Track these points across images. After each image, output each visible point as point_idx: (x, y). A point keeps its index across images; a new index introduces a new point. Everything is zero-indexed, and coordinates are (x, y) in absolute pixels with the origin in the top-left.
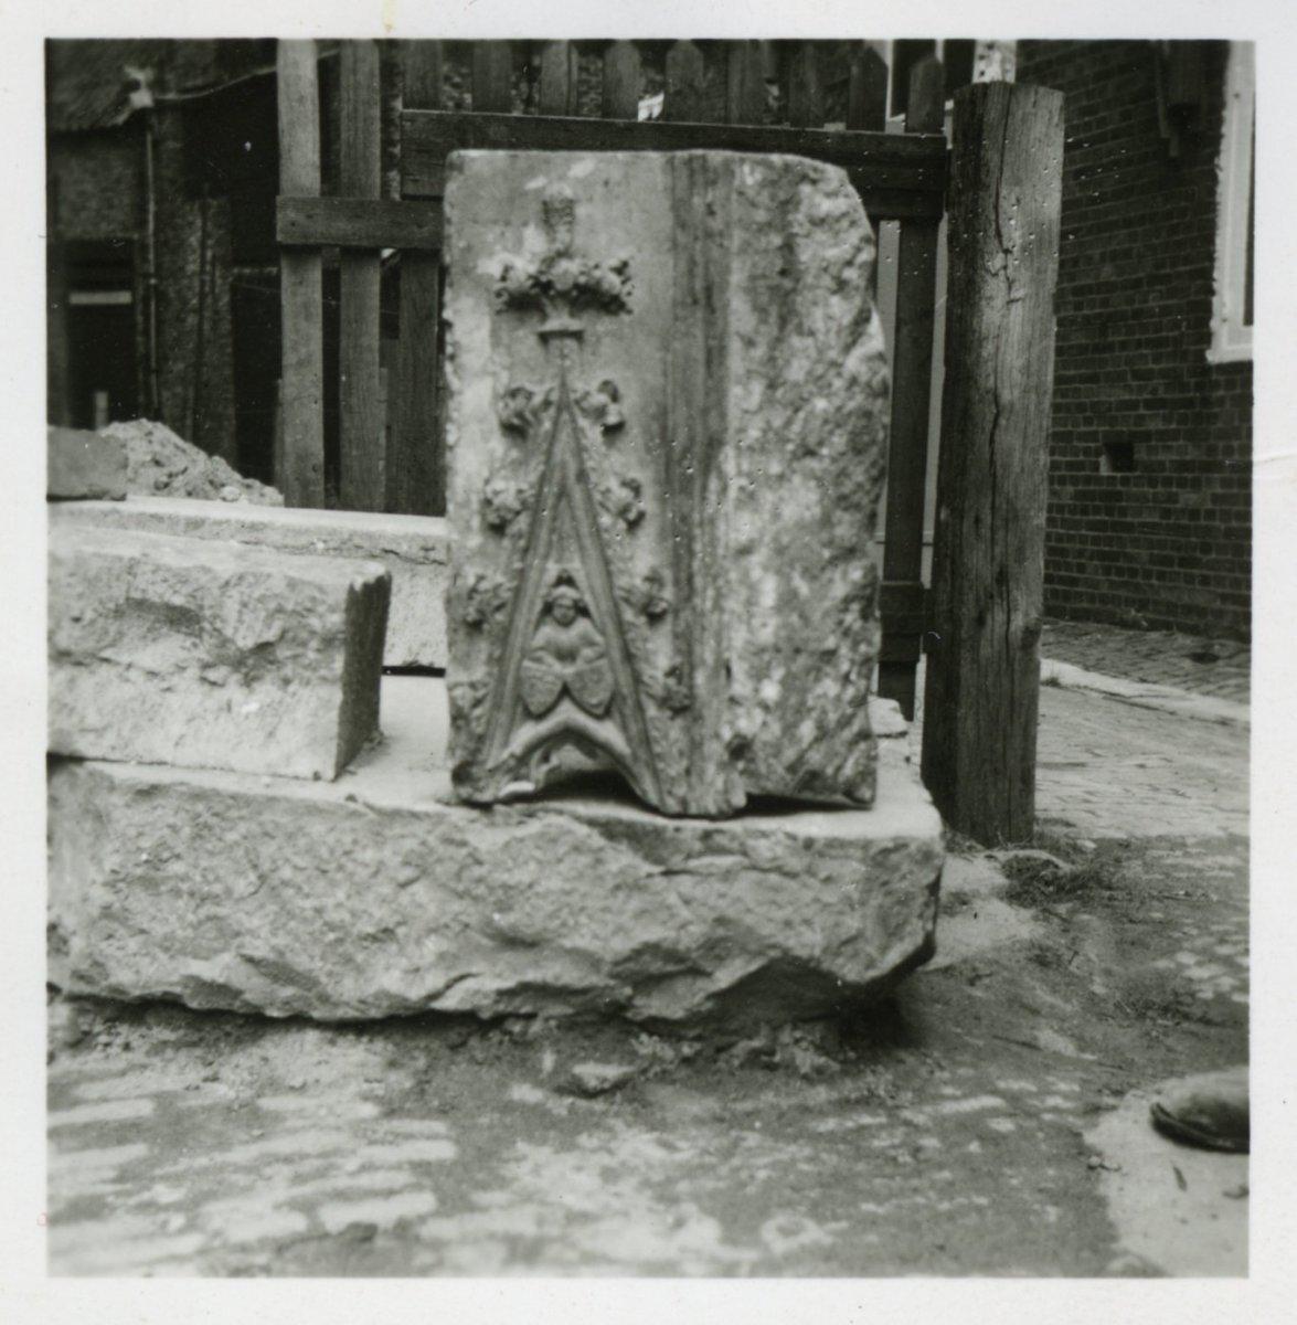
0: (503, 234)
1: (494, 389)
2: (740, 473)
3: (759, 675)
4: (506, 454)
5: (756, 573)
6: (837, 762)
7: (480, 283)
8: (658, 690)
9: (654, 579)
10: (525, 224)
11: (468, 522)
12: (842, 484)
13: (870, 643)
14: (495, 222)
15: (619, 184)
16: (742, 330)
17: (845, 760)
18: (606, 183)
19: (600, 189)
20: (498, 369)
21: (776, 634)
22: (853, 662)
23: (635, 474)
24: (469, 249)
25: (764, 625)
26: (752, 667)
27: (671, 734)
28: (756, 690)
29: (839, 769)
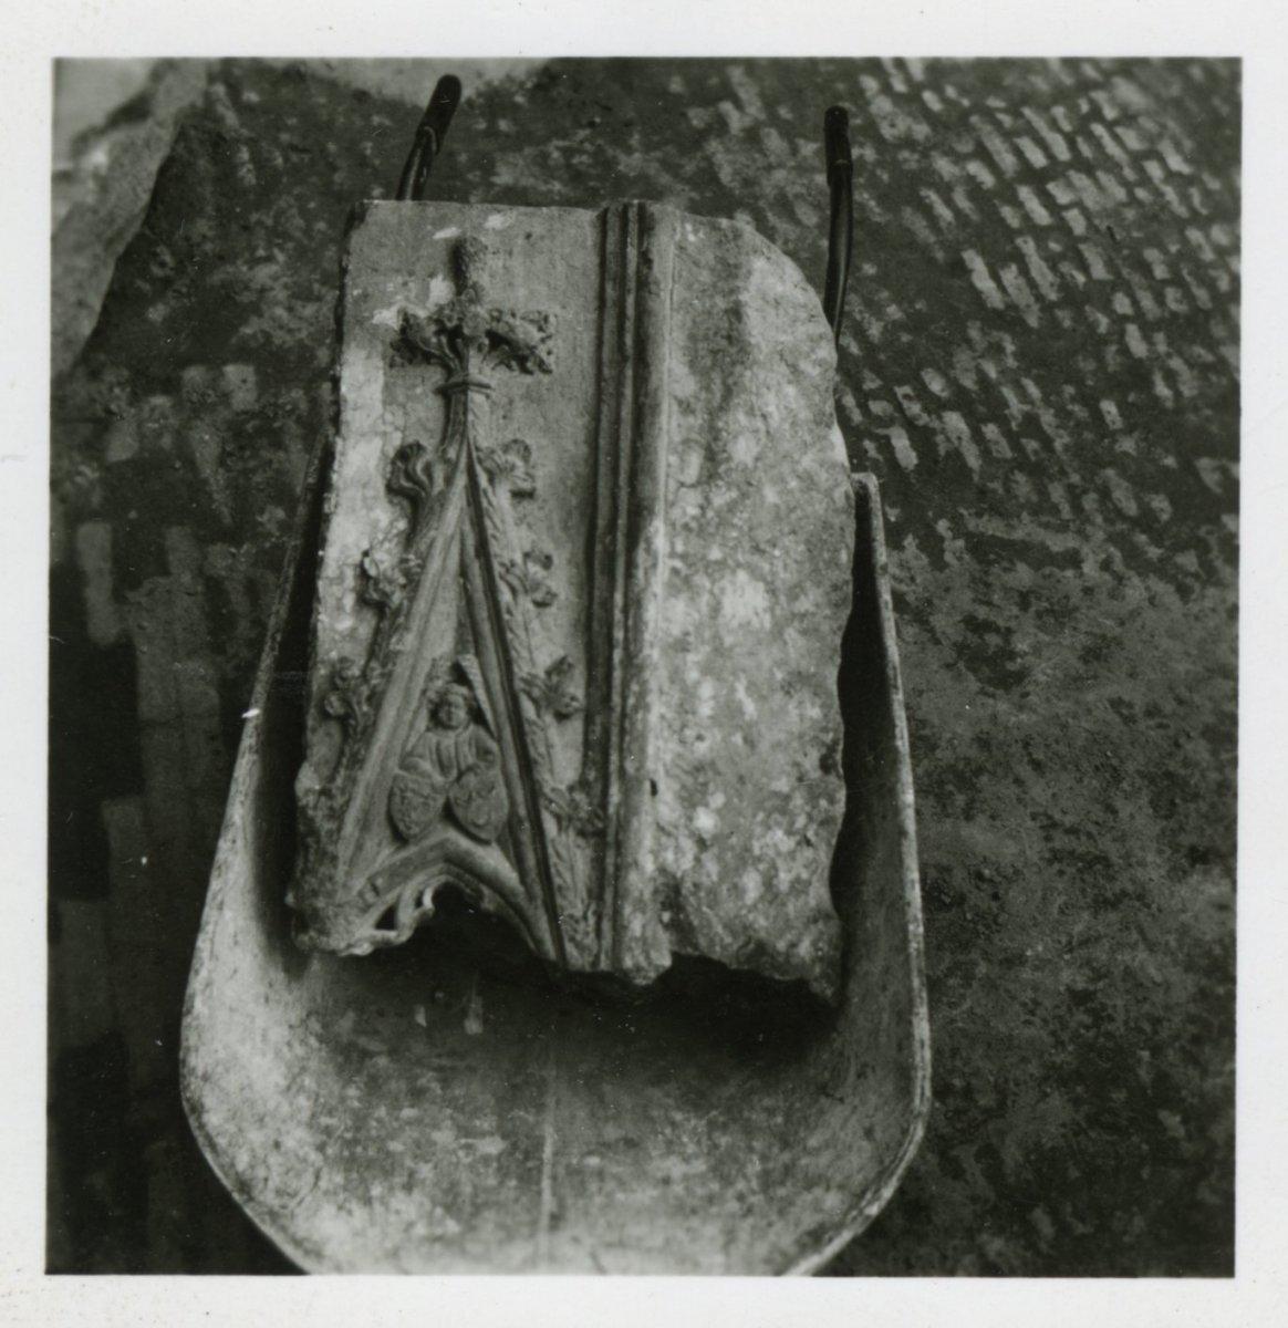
0: (405, 284)
1: (383, 453)
2: (673, 554)
3: (691, 799)
4: (391, 523)
5: (693, 675)
6: (789, 937)
7: (374, 332)
8: (561, 805)
9: (560, 668)
10: (432, 275)
11: (340, 600)
12: (796, 598)
13: (832, 801)
14: (398, 271)
15: (542, 238)
16: (680, 394)
17: (801, 935)
18: (528, 236)
19: (520, 241)
20: (389, 429)
21: (711, 749)
22: (810, 818)
23: (548, 547)
24: (365, 296)
25: (700, 738)
26: (684, 787)
27: (572, 860)
28: (690, 819)
29: (793, 945)
